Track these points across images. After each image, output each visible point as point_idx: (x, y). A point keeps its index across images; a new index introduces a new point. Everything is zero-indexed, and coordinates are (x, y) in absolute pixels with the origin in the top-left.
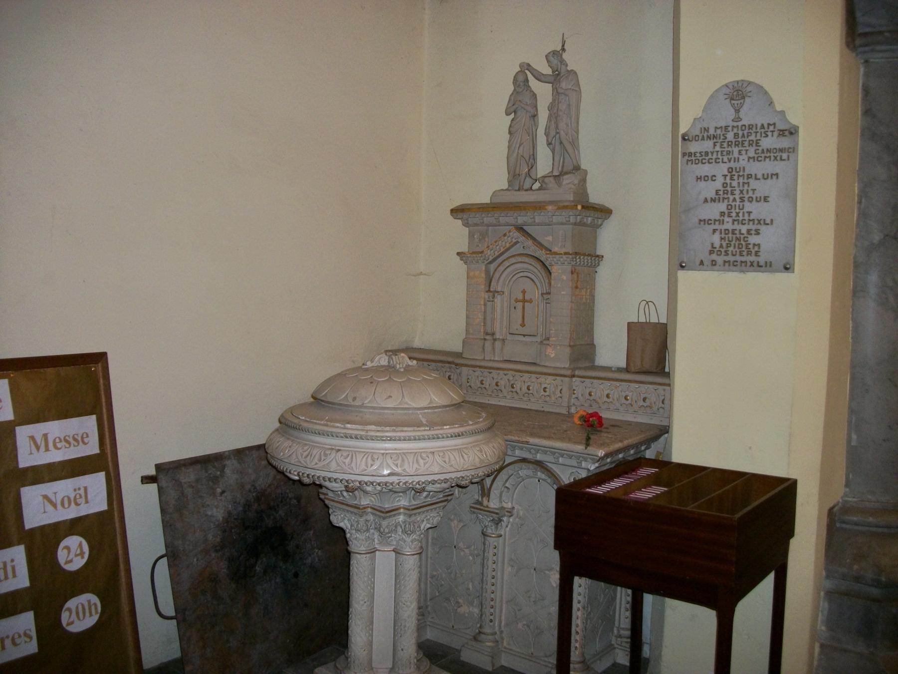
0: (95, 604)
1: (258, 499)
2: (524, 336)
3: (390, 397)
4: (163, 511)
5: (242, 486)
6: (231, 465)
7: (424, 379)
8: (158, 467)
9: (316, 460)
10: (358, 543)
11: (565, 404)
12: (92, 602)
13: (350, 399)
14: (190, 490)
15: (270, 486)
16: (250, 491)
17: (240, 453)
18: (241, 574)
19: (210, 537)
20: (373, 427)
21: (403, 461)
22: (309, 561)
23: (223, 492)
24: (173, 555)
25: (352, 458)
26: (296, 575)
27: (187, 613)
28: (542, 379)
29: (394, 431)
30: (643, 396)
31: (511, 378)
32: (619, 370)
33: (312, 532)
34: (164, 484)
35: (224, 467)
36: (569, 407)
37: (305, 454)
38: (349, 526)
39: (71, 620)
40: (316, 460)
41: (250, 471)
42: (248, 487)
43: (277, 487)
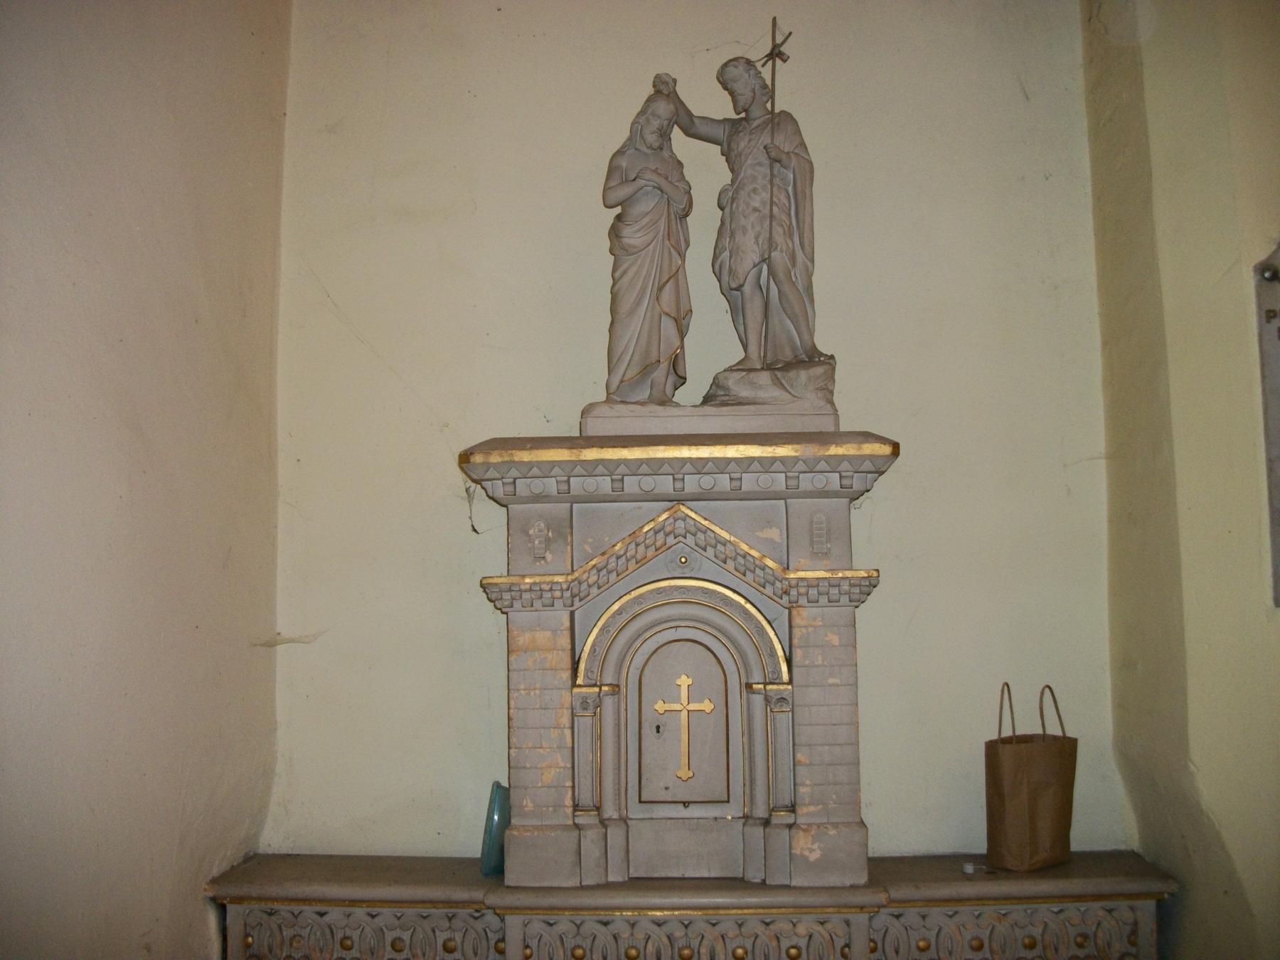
2: (686, 804)
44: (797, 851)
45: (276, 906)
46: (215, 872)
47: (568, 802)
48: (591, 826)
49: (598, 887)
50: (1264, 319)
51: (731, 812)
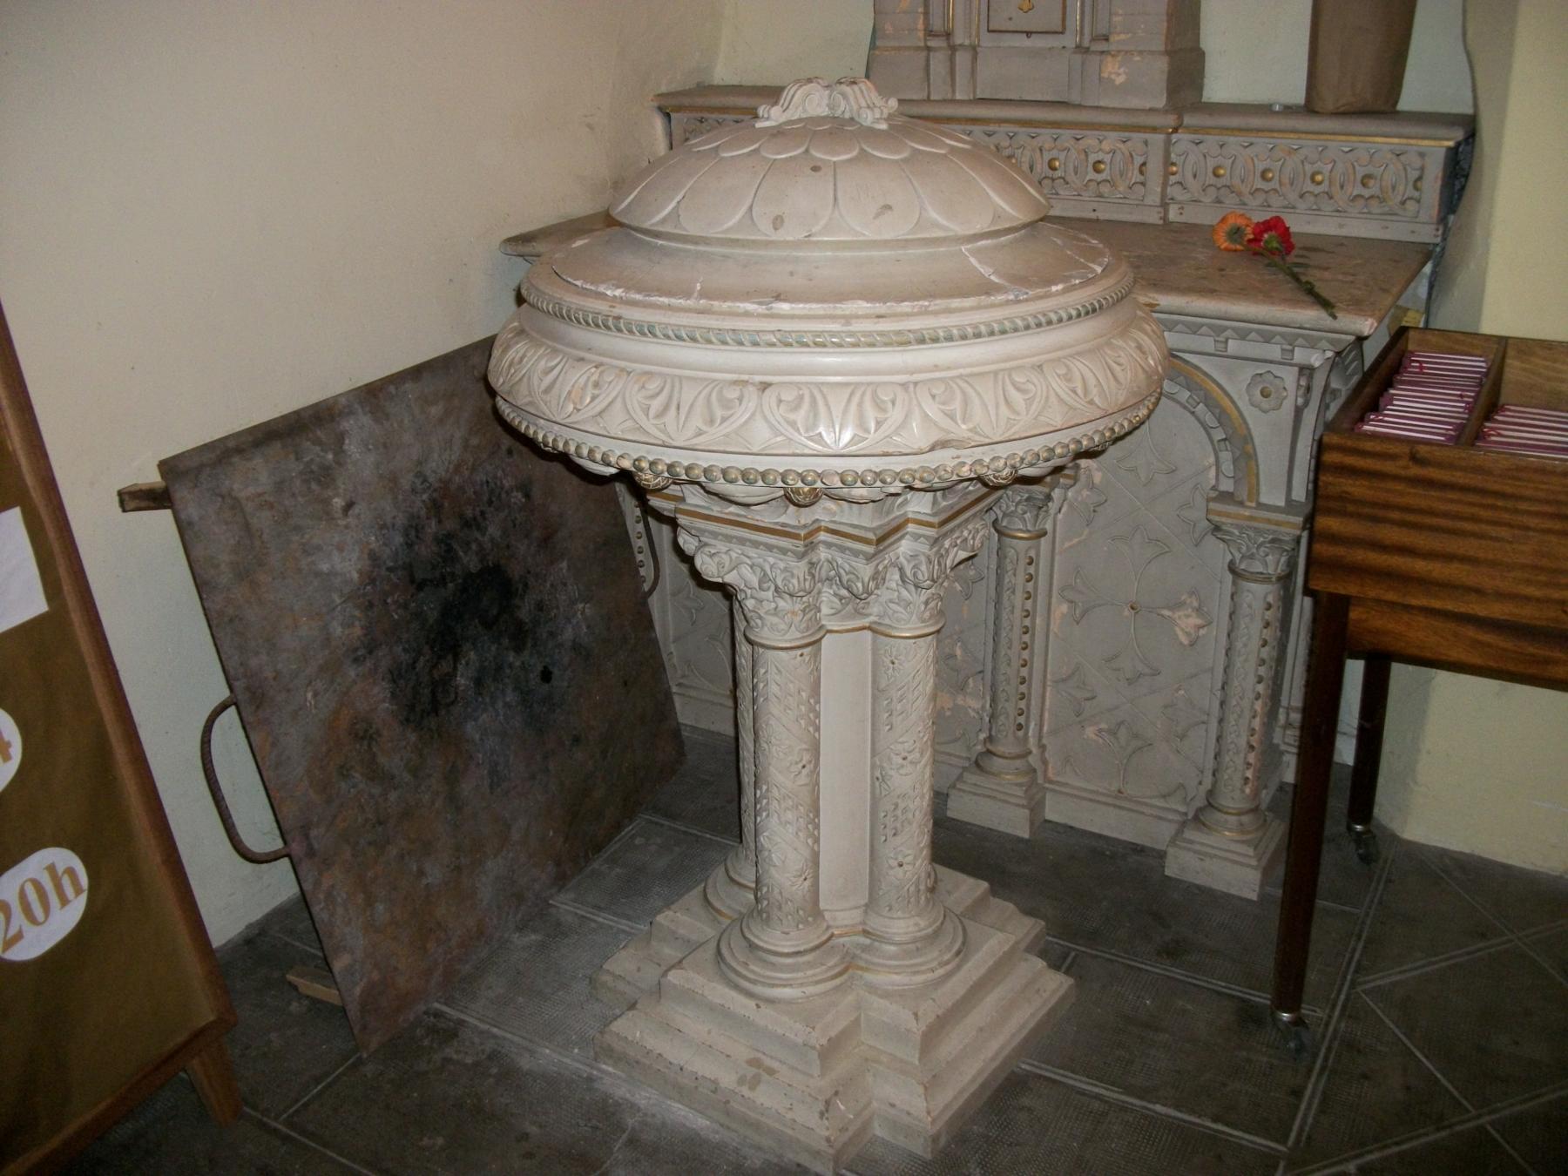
0: (71, 872)
1: (435, 507)
2: (1029, 34)
3: (888, 207)
4: (202, 586)
5: (394, 480)
6: (358, 427)
7: (953, 149)
8: (166, 467)
9: (697, 422)
10: (774, 623)
11: (1154, 198)
12: (60, 869)
13: (765, 226)
14: (266, 514)
15: (457, 469)
16: (414, 491)
17: (373, 395)
18: (426, 704)
19: (337, 630)
20: (862, 306)
21: (966, 401)
22: (568, 634)
23: (349, 506)
24: (249, 697)
25: (814, 402)
26: (546, 676)
27: (314, 833)
28: (1090, 140)
29: (925, 312)
30: (1361, 172)
31: (1005, 143)
32: (1289, 110)
33: (564, 565)
34: (192, 512)
35: (340, 438)
36: (1164, 205)
37: (656, 405)
38: (755, 581)
39: (13, 931)
40: (697, 422)
41: (407, 438)
42: (406, 482)
43: (473, 469)
44: (1105, 75)
45: (706, 115)
46: (663, 89)
47: (920, 26)
48: (940, 48)
49: (970, 102)
50: (1023, 945)
51: (1069, 40)
